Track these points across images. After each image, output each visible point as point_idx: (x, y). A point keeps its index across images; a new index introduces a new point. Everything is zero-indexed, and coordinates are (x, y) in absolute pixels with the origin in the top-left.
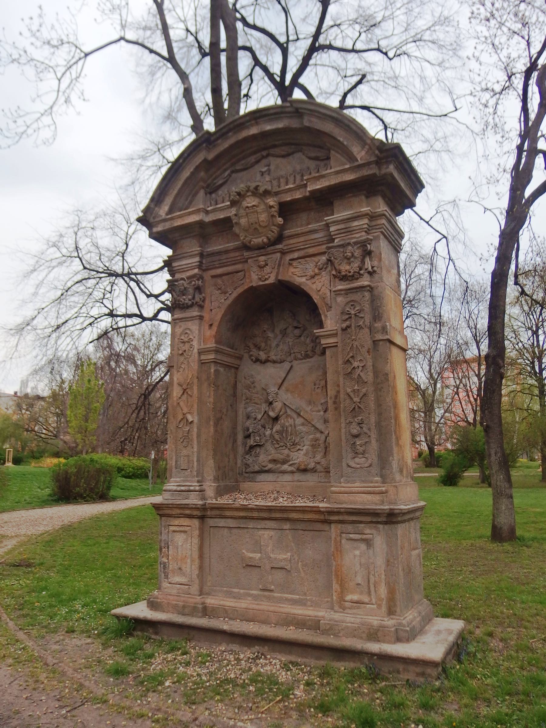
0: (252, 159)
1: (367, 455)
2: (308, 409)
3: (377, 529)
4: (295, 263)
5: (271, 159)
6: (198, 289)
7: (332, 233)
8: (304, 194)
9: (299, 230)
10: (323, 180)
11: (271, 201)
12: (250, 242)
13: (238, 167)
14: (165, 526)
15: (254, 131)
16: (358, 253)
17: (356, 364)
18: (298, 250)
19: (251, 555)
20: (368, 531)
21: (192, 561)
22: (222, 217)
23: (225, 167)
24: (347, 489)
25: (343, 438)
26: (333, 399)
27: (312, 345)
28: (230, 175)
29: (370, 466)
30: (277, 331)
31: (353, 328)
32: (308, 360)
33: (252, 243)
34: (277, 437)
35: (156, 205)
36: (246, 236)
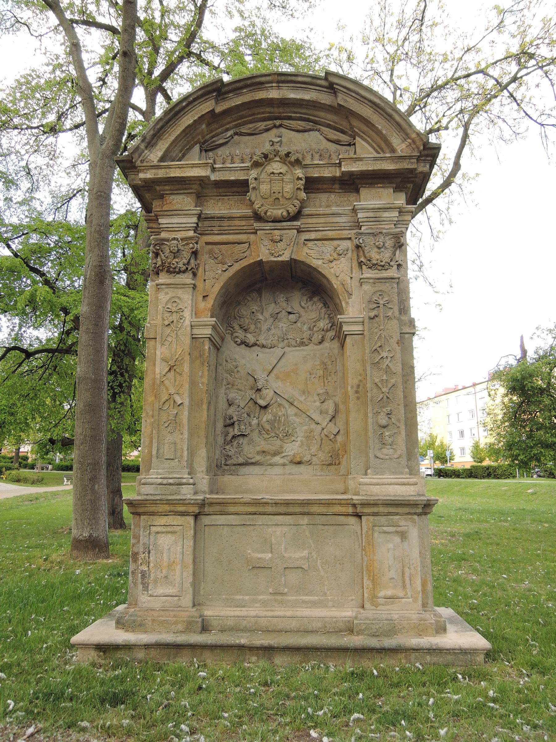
0: (262, 125)
1: (395, 447)
2: (302, 398)
3: (413, 521)
4: (310, 244)
5: (282, 130)
6: (195, 254)
7: (360, 220)
9: (321, 210)
10: (361, 163)
11: (299, 172)
13: (244, 130)
14: (145, 527)
15: (274, 94)
16: (389, 243)
17: (384, 354)
19: (260, 556)
20: (403, 523)
21: (184, 567)
22: (233, 178)
23: (228, 126)
24: (379, 481)
25: (370, 428)
26: (355, 389)
27: (309, 332)
28: (232, 137)
30: (267, 314)
31: (382, 318)
32: (302, 348)
33: (268, 214)
34: (267, 427)
35: (146, 148)
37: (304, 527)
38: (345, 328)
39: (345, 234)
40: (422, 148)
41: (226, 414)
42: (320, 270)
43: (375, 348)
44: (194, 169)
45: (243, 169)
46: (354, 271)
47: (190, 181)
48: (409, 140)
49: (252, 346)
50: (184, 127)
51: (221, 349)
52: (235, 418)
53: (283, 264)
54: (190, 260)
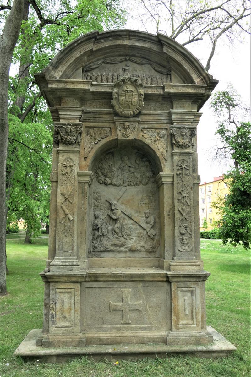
0: (119, 59)
3: (198, 285)
4: (145, 131)
8: (160, 92)
9: (152, 112)
10: (175, 88)
11: (142, 91)
12: (121, 112)
14: (53, 290)
15: (127, 42)
17: (184, 195)
18: (148, 123)
19: (116, 304)
20: (193, 286)
21: (75, 311)
22: (103, 91)
24: (178, 263)
26: (168, 213)
29: (192, 250)
32: (136, 187)
33: (123, 113)
34: (117, 231)
36: (120, 108)
37: (140, 288)
38: (163, 179)
39: (164, 126)
40: (209, 82)
41: (94, 223)
42: (150, 146)
43: (179, 191)
44: (81, 84)
45: (109, 86)
46: (168, 148)
47: (78, 90)
48: (201, 77)
49: (109, 185)
50: (75, 58)
51: (91, 186)
52: (99, 226)
53: (130, 142)
54: (77, 137)
